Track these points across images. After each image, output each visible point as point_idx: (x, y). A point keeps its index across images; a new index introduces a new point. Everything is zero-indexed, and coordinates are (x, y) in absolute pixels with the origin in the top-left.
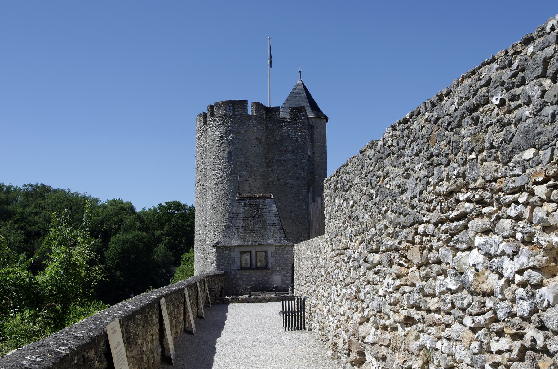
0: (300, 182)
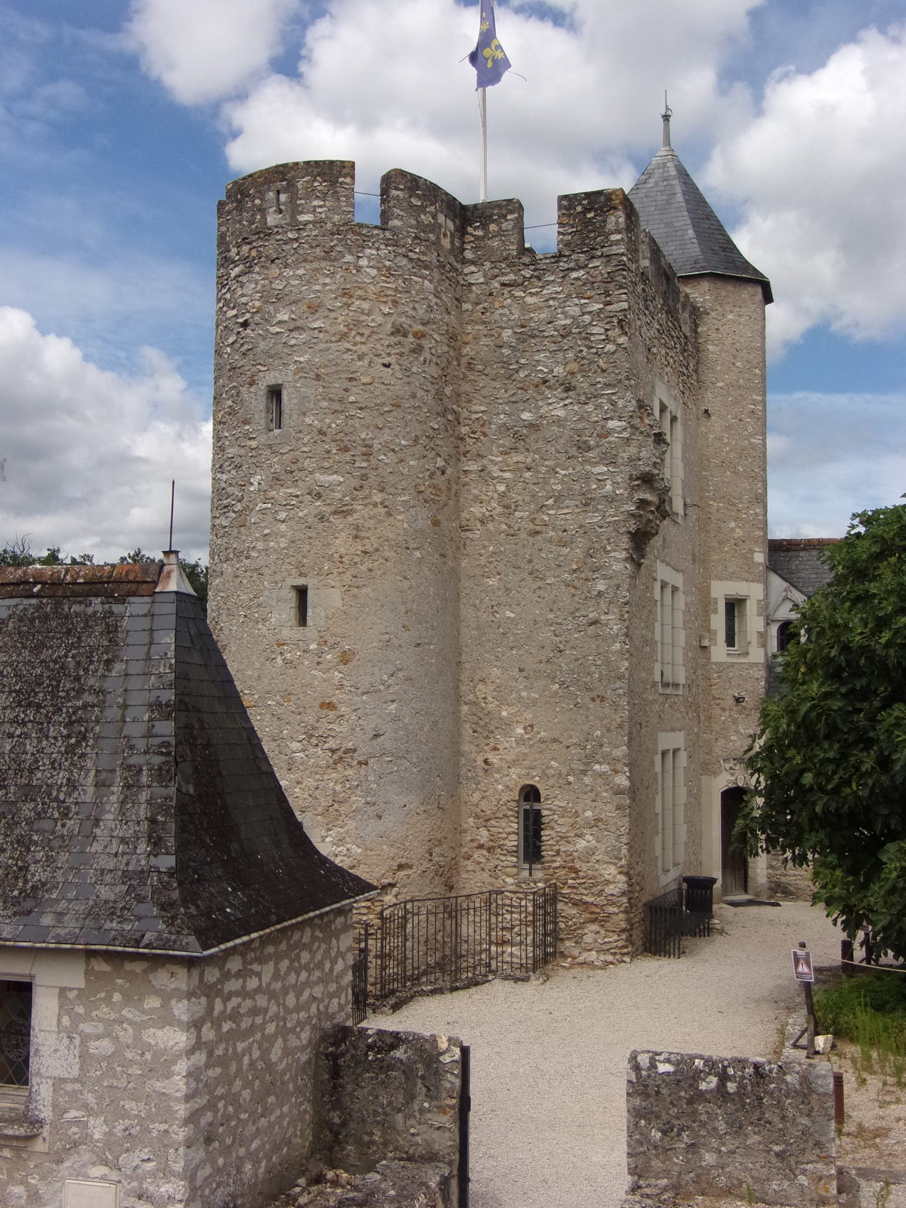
0: (596, 518)
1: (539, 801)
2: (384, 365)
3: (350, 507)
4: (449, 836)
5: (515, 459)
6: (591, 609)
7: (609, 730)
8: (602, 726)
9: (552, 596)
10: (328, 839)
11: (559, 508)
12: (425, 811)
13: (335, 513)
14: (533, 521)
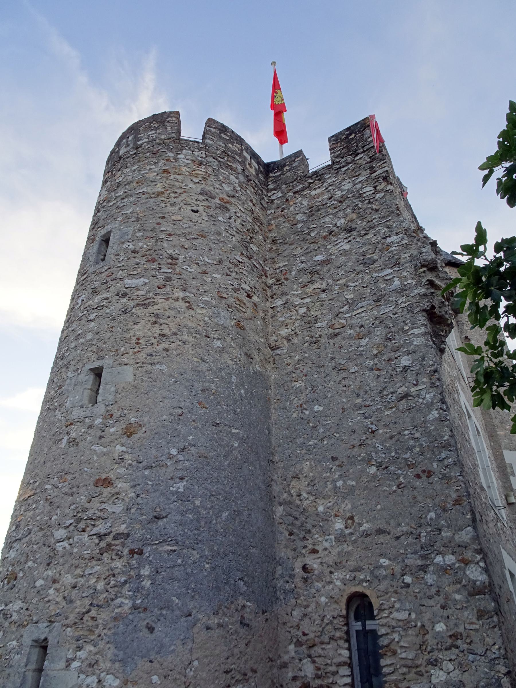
1: (372, 617)
2: (193, 211)
3: (153, 300)
4: (261, 669)
5: (312, 288)
6: (398, 385)
7: (444, 510)
8: (435, 505)
9: (357, 382)
10: (75, 664)
11: (354, 310)
12: (219, 625)
13: (137, 305)
14: (332, 326)
